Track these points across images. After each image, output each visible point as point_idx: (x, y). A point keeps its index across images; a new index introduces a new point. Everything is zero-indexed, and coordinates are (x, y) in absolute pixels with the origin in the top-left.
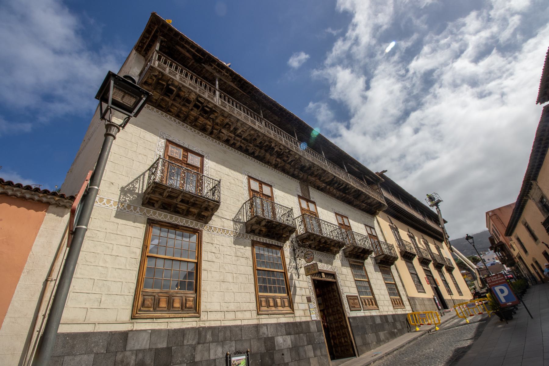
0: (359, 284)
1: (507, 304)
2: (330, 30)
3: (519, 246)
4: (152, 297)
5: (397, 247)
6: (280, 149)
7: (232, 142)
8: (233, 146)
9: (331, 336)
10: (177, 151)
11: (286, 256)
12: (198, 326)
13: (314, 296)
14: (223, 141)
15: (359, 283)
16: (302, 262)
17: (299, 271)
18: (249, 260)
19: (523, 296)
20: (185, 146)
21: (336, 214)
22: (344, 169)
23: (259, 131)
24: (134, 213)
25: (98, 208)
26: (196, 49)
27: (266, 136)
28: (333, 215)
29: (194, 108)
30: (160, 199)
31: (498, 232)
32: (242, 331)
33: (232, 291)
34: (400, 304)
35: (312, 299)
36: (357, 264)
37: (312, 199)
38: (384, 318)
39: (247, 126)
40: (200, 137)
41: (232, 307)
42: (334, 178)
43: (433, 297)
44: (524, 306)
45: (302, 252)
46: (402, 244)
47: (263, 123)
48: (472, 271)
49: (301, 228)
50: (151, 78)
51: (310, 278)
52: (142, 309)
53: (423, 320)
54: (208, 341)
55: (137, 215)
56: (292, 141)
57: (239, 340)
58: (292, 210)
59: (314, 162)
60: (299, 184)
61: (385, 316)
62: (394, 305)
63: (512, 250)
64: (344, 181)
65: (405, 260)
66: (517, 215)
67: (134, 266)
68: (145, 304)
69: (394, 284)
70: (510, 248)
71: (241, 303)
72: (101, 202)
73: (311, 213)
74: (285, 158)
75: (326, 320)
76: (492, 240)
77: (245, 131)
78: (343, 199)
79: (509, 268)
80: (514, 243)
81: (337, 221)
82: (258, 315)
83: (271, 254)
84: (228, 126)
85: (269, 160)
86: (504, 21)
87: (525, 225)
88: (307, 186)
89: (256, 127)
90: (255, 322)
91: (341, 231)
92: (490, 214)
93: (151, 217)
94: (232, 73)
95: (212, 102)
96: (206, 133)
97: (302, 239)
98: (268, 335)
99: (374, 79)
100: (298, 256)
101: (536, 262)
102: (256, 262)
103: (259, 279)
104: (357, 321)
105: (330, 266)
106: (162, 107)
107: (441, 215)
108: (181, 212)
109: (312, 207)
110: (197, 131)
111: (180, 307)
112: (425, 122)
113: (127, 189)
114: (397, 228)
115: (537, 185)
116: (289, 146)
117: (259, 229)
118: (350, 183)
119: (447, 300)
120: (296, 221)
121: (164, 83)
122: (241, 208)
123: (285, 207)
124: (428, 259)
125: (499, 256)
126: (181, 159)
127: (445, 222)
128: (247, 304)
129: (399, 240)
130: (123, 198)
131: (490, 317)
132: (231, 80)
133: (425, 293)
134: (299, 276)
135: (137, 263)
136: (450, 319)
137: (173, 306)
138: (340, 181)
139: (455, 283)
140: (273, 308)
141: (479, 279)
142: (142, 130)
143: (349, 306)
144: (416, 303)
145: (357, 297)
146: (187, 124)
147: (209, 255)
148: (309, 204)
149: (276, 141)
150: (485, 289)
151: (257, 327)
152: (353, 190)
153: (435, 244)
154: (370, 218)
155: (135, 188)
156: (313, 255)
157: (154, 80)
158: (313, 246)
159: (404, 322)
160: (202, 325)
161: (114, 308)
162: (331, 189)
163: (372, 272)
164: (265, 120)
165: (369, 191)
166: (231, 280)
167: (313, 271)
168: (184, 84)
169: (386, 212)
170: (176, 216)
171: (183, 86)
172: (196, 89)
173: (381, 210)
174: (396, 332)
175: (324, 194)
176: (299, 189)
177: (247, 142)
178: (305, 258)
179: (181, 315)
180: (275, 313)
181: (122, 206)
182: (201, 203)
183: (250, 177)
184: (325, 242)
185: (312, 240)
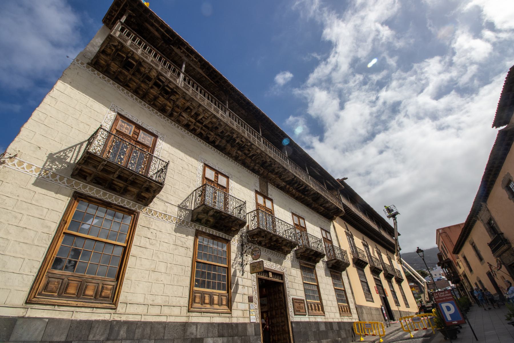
0: (307, 287)
1: (453, 323)
2: (315, 55)
3: (465, 264)
4: (59, 280)
5: (351, 254)
6: (242, 141)
7: (192, 127)
8: (193, 131)
9: (271, 340)
10: (128, 127)
11: (232, 250)
12: (112, 319)
13: (257, 296)
14: (182, 125)
15: (307, 287)
16: (249, 259)
17: (244, 268)
18: (189, 250)
19: (467, 313)
20: (138, 123)
21: (293, 214)
22: (306, 171)
23: (221, 120)
24: (59, 183)
25: (14, 171)
26: (166, 29)
27: (228, 126)
28: (289, 215)
29: (154, 86)
30: (93, 172)
31: (446, 249)
32: (166, 329)
33: (162, 283)
34: (347, 311)
35: (254, 300)
36: (308, 266)
37: (269, 196)
38: (329, 325)
39: (209, 113)
40: (158, 117)
41: (159, 300)
42: (294, 178)
43: (380, 307)
44: (469, 326)
45: (250, 248)
46: (355, 251)
47: (227, 113)
48: (420, 283)
49: (253, 223)
50: (110, 48)
51: (255, 276)
52: (43, 293)
53: (368, 330)
54: (120, 338)
55: (63, 185)
56: (255, 135)
57: (159, 339)
58: (245, 203)
59: (276, 159)
60: (258, 180)
61: (331, 323)
62: (341, 312)
63: (458, 268)
64: (303, 182)
65: (356, 268)
66: (465, 234)
67: (44, 242)
68: (49, 287)
69: (343, 290)
70: (457, 266)
71: (170, 297)
72: (19, 165)
73: (266, 210)
74: (247, 152)
75: (269, 323)
76: (440, 256)
77: (207, 118)
78: (302, 200)
79: (453, 285)
80: (461, 261)
81: (292, 221)
82: (189, 312)
83: (215, 247)
84: (189, 110)
85: (229, 151)
86: (465, 67)
87: (472, 244)
88: (267, 183)
89: (219, 116)
90: (183, 320)
91: (295, 231)
92: (440, 231)
93: (79, 190)
94: (201, 60)
95: (174, 82)
96: (165, 114)
97: (252, 235)
98: (197, 335)
99: (348, 103)
100: (246, 251)
101: (480, 282)
102: (197, 253)
103: (197, 272)
104: (300, 326)
105: (279, 266)
106: (121, 81)
107: (397, 228)
108: (118, 189)
109: (269, 204)
110: (155, 111)
111: (94, 295)
112: (390, 145)
113: (57, 156)
114: (352, 235)
115: (486, 207)
116: (251, 140)
117: (206, 218)
118: (310, 185)
119: (393, 311)
120: (249, 215)
121: (124, 55)
122: (191, 195)
123: (238, 199)
124: (379, 269)
125: (446, 272)
126: (131, 135)
127: (399, 235)
128: (178, 299)
129: (353, 246)
130: (49, 165)
131: (434, 333)
132: (200, 66)
133: (374, 302)
134: (243, 273)
135: (49, 239)
136: (395, 331)
137: (84, 293)
138: (300, 182)
139: (403, 294)
140: (208, 306)
141: (426, 292)
142: (91, 99)
143: (294, 310)
144: (363, 311)
145: (303, 300)
146: (145, 102)
147: (142, 240)
148: (266, 200)
149: (239, 133)
150: (431, 303)
151: (185, 325)
152: (312, 193)
153: (388, 255)
154: (327, 222)
155: (67, 156)
156: (260, 252)
157: (113, 50)
158: (263, 243)
159: (349, 330)
160: (117, 318)
161: (6, 288)
162: (290, 188)
163: (322, 275)
164: (229, 111)
165: (328, 195)
166: (163, 270)
167: (258, 269)
168: (145, 59)
169: (342, 218)
170: (111, 194)
171: (143, 61)
172: (158, 67)
173: (338, 216)
174: (339, 341)
175: (283, 193)
176: (258, 185)
177: (208, 129)
178: (252, 254)
179: (92, 304)
180: (209, 311)
181: (45, 174)
182: (141, 183)
183: (206, 165)
184: (277, 241)
185: (263, 237)
